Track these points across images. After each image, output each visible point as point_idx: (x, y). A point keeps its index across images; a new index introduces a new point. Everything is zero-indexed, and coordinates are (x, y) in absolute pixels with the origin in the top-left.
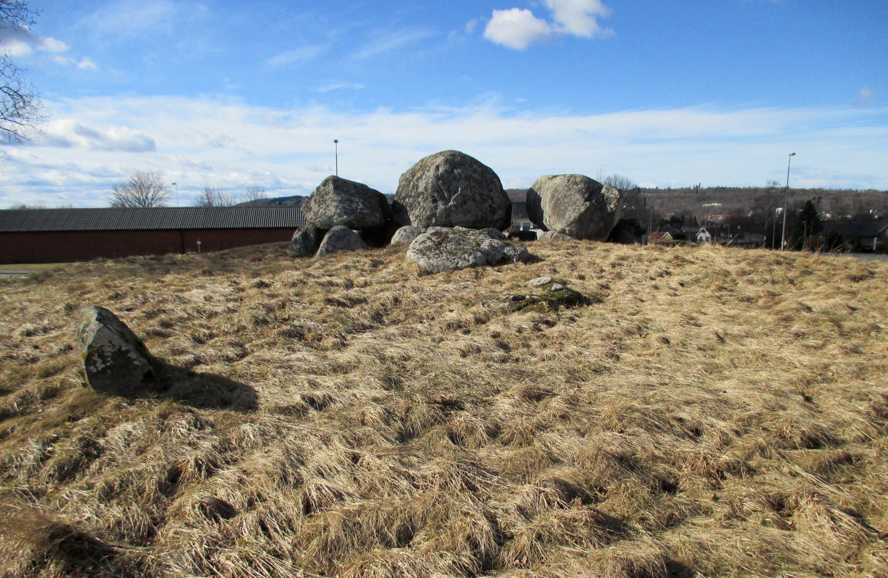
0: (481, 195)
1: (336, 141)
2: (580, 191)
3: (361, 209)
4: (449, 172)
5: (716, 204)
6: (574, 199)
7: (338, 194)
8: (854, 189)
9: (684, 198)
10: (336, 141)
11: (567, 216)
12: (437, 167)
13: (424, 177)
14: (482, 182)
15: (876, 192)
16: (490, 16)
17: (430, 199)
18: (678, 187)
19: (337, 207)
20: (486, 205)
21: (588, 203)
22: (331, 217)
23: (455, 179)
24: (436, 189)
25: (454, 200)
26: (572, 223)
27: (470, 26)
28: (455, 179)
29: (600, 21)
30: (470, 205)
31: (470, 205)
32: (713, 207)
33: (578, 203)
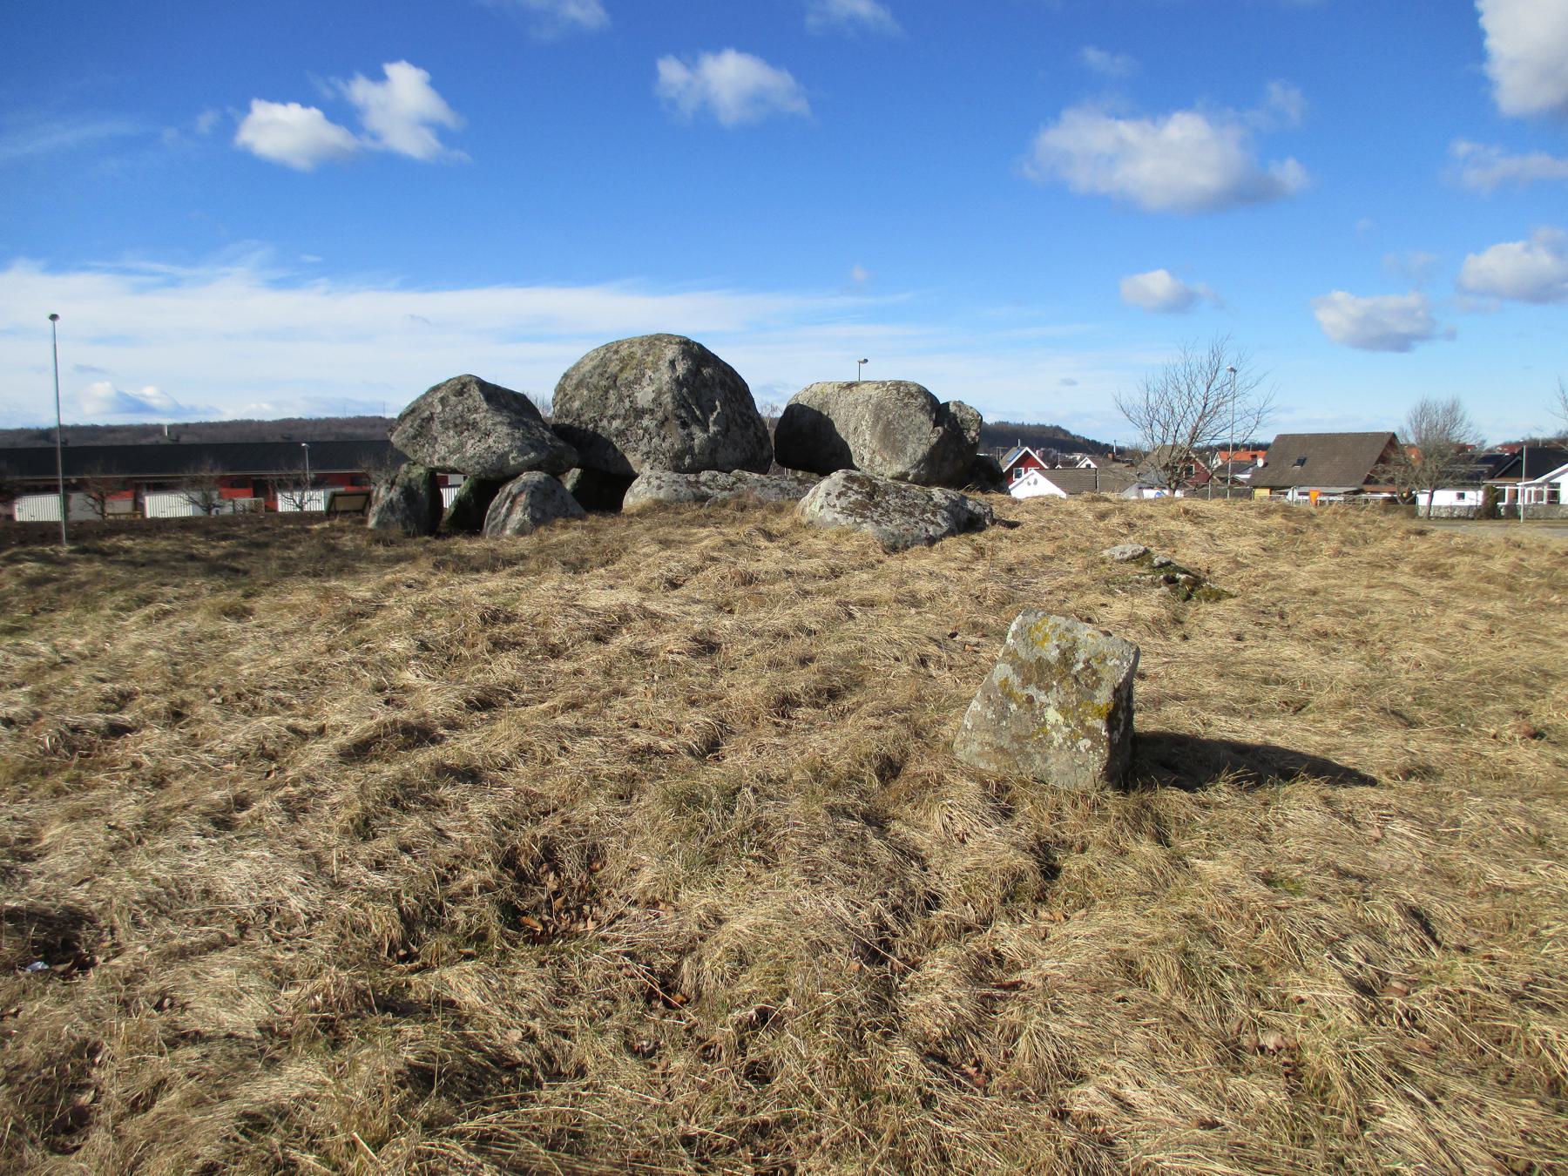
2: (923, 408)
6: (917, 421)
8: (256, 418)
10: (54, 317)
11: (910, 450)
12: (672, 363)
13: (645, 382)
16: (247, 110)
22: (504, 455)
23: (705, 385)
24: (681, 403)
25: (715, 423)
27: (206, 121)
28: (705, 385)
29: (441, 132)
33: (924, 429)
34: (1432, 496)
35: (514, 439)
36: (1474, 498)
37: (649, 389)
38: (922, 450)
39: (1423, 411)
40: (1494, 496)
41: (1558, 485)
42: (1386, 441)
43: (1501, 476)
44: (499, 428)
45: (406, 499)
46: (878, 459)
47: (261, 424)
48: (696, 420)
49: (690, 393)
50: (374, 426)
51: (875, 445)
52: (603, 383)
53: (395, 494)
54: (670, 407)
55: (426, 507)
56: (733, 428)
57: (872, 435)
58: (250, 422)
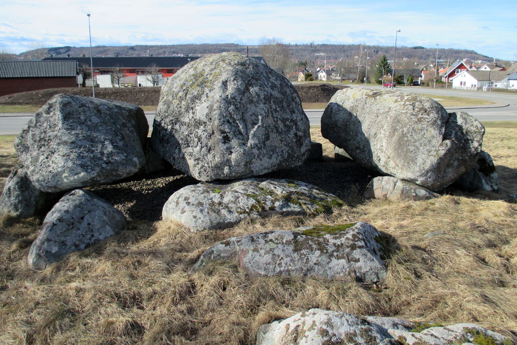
0: (284, 121)
1: (89, 15)
2: (434, 123)
3: (110, 154)
4: (243, 92)
5: (322, 54)
6: (428, 135)
7: (70, 128)
9: (304, 50)
10: (89, 15)
11: (420, 161)
12: (225, 84)
13: (204, 98)
14: (282, 102)
15: (406, 47)
17: (218, 136)
18: (301, 44)
19: (66, 156)
20: (291, 135)
21: (448, 142)
23: (251, 102)
24: (227, 120)
25: (254, 135)
26: (427, 172)
28: (251, 102)
30: (275, 139)
31: (275, 139)
32: (321, 55)
33: (434, 142)
38: (431, 161)
45: (20, 188)
47: (196, 45)
48: (238, 133)
50: (231, 47)
51: (390, 152)
54: (216, 123)
56: (273, 135)
57: (388, 143)
58: (193, 45)
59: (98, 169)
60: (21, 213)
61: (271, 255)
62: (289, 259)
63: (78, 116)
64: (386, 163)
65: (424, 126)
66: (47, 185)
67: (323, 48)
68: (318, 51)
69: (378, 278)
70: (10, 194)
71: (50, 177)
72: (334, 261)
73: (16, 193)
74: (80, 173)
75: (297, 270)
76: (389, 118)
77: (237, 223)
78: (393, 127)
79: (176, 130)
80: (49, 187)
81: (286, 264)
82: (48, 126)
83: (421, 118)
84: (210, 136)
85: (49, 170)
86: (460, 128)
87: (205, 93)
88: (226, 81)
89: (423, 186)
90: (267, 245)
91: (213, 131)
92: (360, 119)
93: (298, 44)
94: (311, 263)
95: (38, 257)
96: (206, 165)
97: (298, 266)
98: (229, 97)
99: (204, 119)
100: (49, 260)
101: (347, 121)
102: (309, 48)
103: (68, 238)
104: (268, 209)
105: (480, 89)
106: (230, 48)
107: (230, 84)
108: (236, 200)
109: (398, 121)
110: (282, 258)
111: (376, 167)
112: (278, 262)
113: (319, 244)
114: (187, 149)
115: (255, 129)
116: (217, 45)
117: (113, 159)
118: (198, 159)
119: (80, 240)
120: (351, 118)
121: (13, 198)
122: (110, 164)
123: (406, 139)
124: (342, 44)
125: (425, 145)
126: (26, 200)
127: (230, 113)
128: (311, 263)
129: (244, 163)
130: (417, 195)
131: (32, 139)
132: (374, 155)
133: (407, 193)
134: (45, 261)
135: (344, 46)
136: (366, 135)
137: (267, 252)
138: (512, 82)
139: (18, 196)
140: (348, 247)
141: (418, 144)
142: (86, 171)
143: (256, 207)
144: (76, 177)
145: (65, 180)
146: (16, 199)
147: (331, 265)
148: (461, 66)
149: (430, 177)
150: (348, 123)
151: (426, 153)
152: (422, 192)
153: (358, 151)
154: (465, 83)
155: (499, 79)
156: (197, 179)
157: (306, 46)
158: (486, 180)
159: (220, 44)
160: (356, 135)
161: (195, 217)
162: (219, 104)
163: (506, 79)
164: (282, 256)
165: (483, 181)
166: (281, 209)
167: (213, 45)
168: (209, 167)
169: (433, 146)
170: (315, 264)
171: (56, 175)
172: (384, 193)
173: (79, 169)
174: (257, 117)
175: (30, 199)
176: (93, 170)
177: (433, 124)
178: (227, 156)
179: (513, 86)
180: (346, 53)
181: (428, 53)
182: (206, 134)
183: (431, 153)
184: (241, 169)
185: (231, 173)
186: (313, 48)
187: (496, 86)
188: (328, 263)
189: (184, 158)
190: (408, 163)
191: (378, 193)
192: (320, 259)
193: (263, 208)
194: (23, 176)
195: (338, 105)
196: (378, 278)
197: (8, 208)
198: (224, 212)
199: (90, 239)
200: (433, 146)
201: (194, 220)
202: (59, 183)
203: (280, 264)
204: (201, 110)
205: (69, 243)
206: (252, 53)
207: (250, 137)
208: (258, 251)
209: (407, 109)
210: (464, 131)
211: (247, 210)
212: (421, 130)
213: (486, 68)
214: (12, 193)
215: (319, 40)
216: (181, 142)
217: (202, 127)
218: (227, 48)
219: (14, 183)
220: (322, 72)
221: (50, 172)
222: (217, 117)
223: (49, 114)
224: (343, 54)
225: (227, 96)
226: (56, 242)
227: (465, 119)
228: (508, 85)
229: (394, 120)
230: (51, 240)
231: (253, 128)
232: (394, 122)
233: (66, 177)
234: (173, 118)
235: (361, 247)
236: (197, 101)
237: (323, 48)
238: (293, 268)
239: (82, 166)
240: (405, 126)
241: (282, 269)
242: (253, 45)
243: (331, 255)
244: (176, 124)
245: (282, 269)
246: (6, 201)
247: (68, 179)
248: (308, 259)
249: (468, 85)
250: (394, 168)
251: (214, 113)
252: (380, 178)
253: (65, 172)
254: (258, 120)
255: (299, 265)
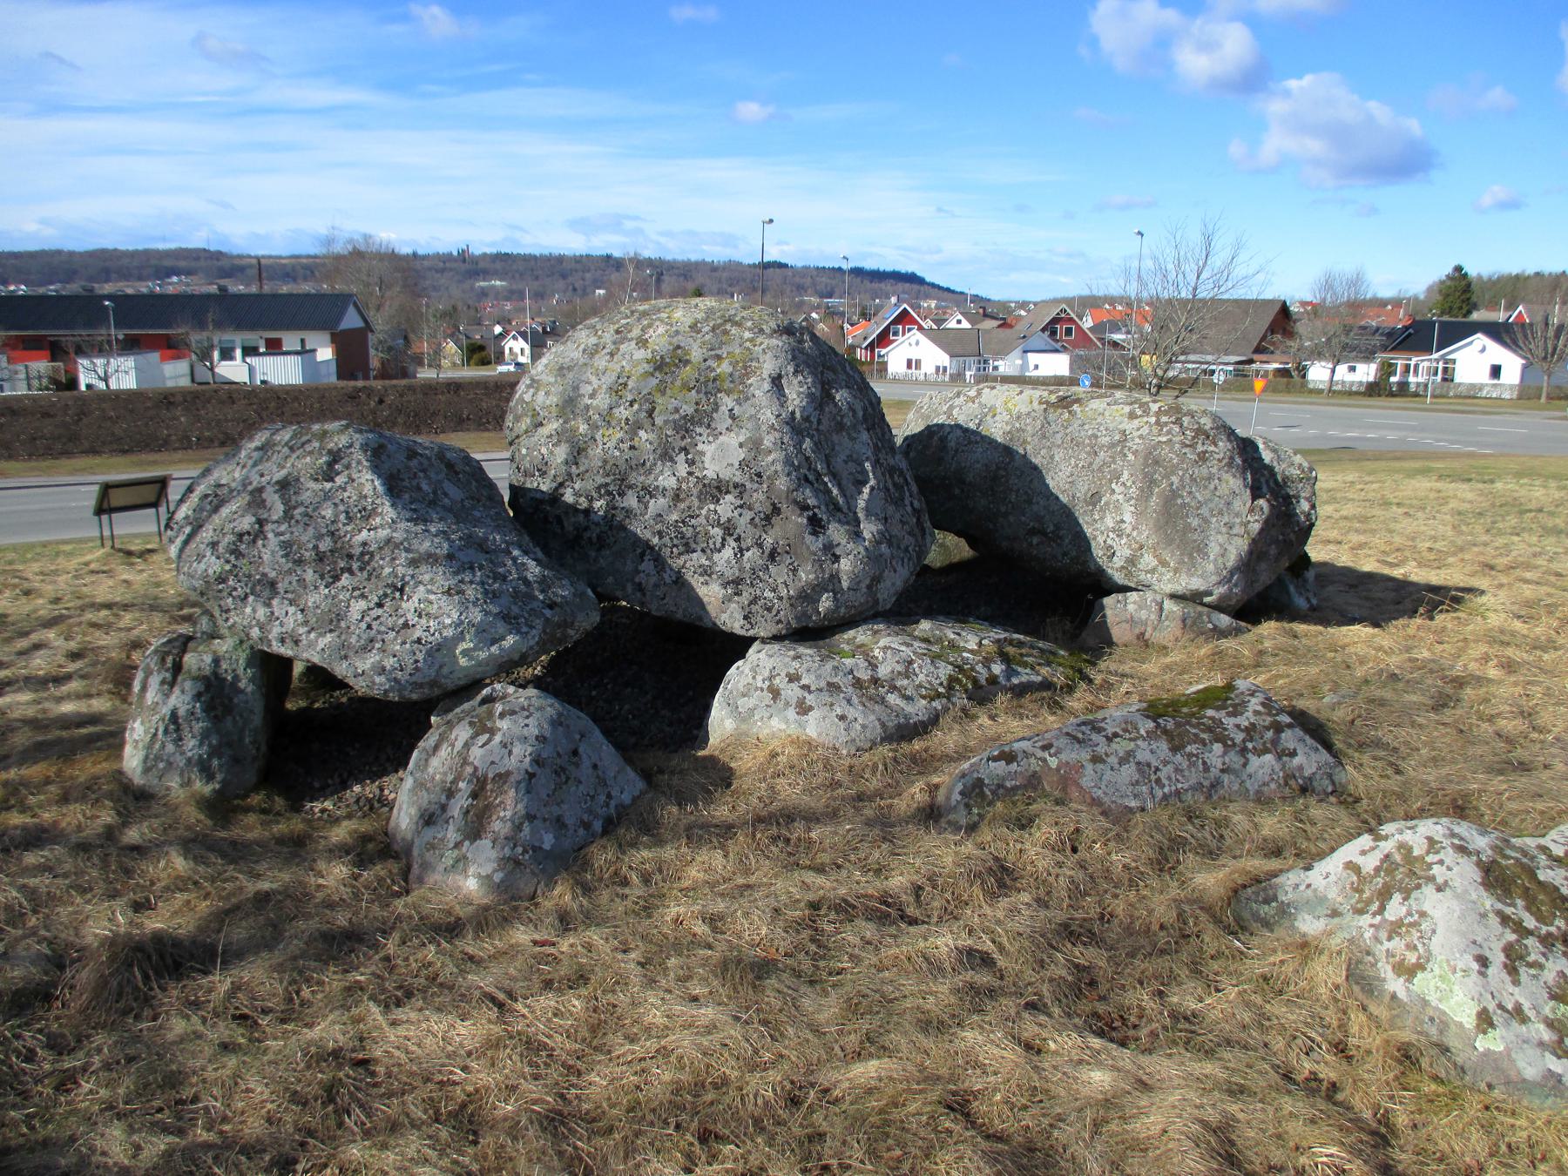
6: (1223, 490)
9: (443, 271)
11: (1214, 550)
12: (776, 381)
13: (722, 420)
21: (1261, 502)
23: (840, 427)
24: (805, 476)
25: (868, 511)
26: (1232, 573)
28: (840, 427)
34: (1333, 371)
35: (464, 606)
36: (1366, 372)
37: (732, 440)
38: (1237, 548)
39: (1328, 285)
40: (1387, 369)
41: (1454, 361)
42: (1277, 308)
43: (1393, 349)
44: (425, 573)
45: (208, 709)
46: (1148, 560)
47: (71, 254)
49: (817, 446)
50: (198, 259)
51: (1145, 534)
52: (623, 412)
53: (180, 700)
54: (782, 484)
55: (257, 720)
57: (1139, 514)
58: (59, 252)
59: (539, 623)
60: (224, 783)
61: (1134, 767)
62: (1170, 768)
63: (414, 483)
64: (1132, 561)
65: (1214, 470)
66: (414, 679)
67: (498, 265)
68: (486, 274)
69: (1333, 783)
70: (178, 730)
71: (420, 656)
72: (1255, 762)
73: (198, 727)
74: (503, 638)
75: (1192, 788)
76: (1131, 457)
77: (934, 720)
78: (1146, 475)
79: (628, 512)
80: (417, 686)
81: (1169, 778)
82: (342, 517)
83: (1205, 452)
84: (768, 518)
85: (415, 637)
86: (1270, 469)
87: (723, 408)
88: (780, 377)
89: (1217, 607)
90: (1114, 746)
91: (774, 504)
92: (1036, 461)
93: (421, 252)
94: (1214, 772)
95: (510, 866)
96: (768, 594)
97: (1193, 781)
98: (798, 415)
99: (731, 474)
100: (543, 871)
101: (998, 468)
102: (454, 265)
103: (565, 807)
104: (984, 682)
105: (958, 377)
106: (193, 264)
107: (790, 383)
108: (907, 668)
109: (1156, 462)
110: (1157, 769)
111: (1101, 572)
112: (1153, 777)
113: (1209, 730)
114: (683, 558)
115: (865, 496)
116: (147, 254)
117: (555, 594)
118: (737, 582)
119: (590, 811)
120: (1012, 459)
121: (190, 743)
122: (557, 609)
123: (1179, 501)
124: (556, 252)
125: (1221, 513)
126: (230, 745)
127: (807, 459)
128: (1214, 772)
129: (867, 582)
130: (1215, 627)
131: (286, 555)
132: (1093, 544)
133: (1194, 623)
134: (533, 873)
135: (561, 259)
136: (1064, 499)
137: (1123, 761)
138: (1033, 358)
139: (205, 736)
140: (1268, 728)
141: (1204, 511)
142: (518, 632)
143: (958, 681)
144: (494, 649)
145: (463, 662)
146: (201, 744)
147: (1250, 769)
148: (903, 318)
149: (1236, 585)
150: (1002, 473)
151: (1224, 530)
152: (1224, 620)
153: (1035, 540)
154: (918, 362)
155: (1003, 353)
156: (742, 632)
157: (446, 258)
158: (1297, 587)
159: (157, 252)
160: (1030, 502)
161: (842, 718)
162: (777, 435)
163: (1017, 352)
164: (1154, 763)
165: (1292, 589)
166: (1009, 679)
167: (133, 254)
168: (781, 598)
169: (1237, 515)
170: (1223, 771)
171: (440, 651)
172: (1137, 631)
173: (501, 627)
174: (861, 464)
175: (241, 739)
176: (532, 627)
177: (1230, 464)
178: (829, 567)
179: (1036, 367)
180: (570, 279)
181: (797, 279)
182: (748, 515)
183: (1235, 531)
184: (860, 598)
185: (837, 607)
186: (467, 266)
187: (996, 368)
188: (1245, 765)
189: (680, 581)
190: (1191, 557)
191: (1118, 632)
192: (1227, 759)
193: (975, 681)
194: (207, 671)
195: (966, 430)
196: (1333, 783)
197: (181, 775)
198: (893, 699)
199: (607, 805)
200: (1237, 515)
201: (842, 725)
202: (445, 671)
203: (1158, 781)
204: (720, 454)
205: (570, 821)
206: (271, 279)
207: (861, 515)
208: (1104, 762)
209: (1169, 432)
210: (1279, 478)
211: (941, 690)
212: (1210, 478)
213: (959, 322)
214: (185, 726)
215: (484, 240)
216: (655, 540)
217: (729, 498)
218: (182, 264)
219: (187, 698)
220: (514, 338)
221: (419, 641)
222: (779, 468)
223: (331, 480)
224: (561, 284)
225: (793, 413)
226: (545, 820)
227: (1274, 451)
228: (1024, 366)
229: (1146, 458)
230: (535, 817)
231: (860, 492)
232: (1146, 466)
233: (465, 653)
234: (608, 480)
235: (1290, 726)
236: (698, 430)
237: (498, 265)
238: (1186, 786)
239: (506, 617)
240: (1173, 473)
241: (1166, 790)
242: (274, 253)
243: (1243, 751)
244: (622, 494)
245: (1166, 790)
246: (170, 755)
247: (471, 658)
248: (1204, 763)
249: (928, 368)
250: (1153, 571)
251: (770, 459)
252: (1120, 596)
253: (463, 639)
254: (864, 472)
255: (1194, 777)
